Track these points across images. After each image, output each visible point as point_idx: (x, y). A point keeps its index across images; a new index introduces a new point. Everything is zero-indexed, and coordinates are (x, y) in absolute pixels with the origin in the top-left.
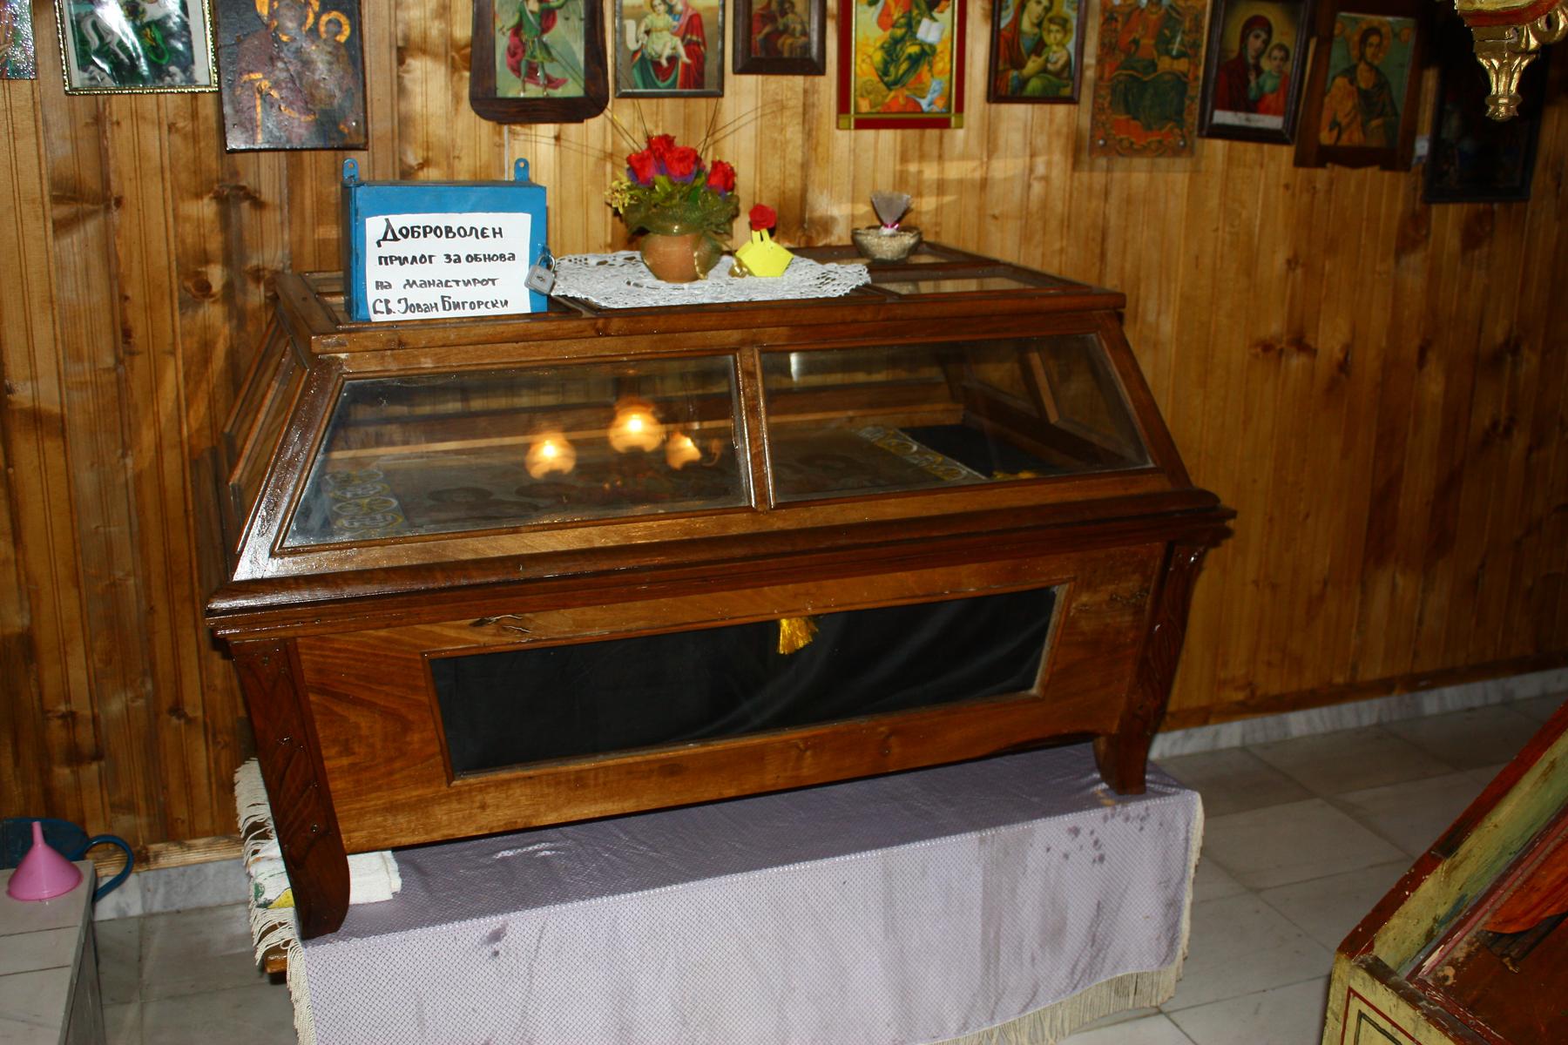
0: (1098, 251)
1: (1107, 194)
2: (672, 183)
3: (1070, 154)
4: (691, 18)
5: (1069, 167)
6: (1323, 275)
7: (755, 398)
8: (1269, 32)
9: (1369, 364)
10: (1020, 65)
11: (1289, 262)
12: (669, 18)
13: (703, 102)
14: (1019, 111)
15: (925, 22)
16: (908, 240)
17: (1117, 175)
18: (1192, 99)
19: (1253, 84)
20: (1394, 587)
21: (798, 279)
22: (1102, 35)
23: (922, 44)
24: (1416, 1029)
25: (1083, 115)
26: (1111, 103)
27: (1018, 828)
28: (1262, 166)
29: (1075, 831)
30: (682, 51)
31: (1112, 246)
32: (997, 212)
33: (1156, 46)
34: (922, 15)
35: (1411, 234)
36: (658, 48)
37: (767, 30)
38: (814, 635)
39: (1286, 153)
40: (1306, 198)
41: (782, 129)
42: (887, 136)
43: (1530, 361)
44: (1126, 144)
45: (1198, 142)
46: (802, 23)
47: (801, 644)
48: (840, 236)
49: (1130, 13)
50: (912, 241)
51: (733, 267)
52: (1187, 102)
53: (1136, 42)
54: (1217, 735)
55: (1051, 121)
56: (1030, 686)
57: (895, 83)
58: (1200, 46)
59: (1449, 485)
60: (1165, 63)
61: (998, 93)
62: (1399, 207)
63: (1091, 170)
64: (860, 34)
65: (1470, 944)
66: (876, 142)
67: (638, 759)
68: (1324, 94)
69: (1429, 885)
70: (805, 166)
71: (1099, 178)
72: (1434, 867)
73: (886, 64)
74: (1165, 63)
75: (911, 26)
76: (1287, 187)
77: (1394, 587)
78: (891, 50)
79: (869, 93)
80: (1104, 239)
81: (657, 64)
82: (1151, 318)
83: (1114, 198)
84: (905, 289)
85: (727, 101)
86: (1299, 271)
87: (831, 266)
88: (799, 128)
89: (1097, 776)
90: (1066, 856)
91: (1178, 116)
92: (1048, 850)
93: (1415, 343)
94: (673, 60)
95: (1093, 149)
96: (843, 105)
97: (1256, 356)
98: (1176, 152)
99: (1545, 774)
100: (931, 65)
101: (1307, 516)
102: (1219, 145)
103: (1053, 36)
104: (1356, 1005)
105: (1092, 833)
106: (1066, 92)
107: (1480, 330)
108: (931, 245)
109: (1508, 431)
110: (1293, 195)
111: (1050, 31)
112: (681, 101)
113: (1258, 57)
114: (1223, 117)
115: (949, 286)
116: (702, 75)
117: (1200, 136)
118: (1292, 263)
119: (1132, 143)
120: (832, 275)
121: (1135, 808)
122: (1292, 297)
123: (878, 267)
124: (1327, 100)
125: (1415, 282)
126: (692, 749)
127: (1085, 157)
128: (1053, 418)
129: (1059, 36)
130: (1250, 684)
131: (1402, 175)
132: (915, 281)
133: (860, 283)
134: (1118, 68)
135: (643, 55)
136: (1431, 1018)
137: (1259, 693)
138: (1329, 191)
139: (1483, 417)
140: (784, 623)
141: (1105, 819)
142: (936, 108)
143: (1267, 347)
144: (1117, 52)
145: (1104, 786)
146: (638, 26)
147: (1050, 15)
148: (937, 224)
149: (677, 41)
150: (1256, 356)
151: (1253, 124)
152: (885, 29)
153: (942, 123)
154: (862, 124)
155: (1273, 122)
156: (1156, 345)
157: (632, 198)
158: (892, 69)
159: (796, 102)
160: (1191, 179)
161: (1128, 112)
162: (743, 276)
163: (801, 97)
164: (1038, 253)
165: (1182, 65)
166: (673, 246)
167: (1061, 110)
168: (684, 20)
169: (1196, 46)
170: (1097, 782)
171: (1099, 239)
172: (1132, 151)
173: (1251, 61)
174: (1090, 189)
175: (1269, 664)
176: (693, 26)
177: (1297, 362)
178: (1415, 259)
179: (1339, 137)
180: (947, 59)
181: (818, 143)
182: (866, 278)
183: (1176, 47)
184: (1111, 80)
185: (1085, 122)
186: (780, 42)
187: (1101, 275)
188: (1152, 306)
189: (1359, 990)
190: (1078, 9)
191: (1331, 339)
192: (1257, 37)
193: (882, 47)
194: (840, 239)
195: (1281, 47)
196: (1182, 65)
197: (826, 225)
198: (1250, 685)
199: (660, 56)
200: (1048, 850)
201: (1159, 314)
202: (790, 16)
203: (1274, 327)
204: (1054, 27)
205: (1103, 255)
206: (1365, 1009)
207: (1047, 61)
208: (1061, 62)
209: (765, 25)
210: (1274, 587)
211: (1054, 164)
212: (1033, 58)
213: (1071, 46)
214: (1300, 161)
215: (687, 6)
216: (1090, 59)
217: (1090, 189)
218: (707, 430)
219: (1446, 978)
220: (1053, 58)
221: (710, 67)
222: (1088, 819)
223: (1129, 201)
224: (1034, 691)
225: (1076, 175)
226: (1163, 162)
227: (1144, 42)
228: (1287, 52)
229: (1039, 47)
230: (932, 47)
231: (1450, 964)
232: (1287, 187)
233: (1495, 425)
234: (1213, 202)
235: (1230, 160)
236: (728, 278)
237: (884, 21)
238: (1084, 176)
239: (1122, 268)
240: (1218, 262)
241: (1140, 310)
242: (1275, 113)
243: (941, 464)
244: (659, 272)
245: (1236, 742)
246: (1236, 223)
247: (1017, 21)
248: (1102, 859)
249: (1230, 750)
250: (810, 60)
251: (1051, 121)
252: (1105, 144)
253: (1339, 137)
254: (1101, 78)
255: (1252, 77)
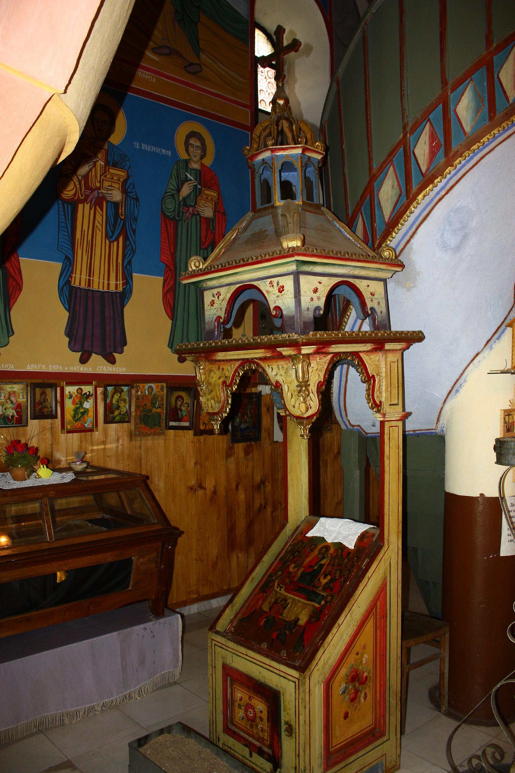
0: (139, 464)
1: (140, 447)
2: (19, 454)
3: (129, 437)
4: (18, 405)
5: (129, 441)
6: (205, 466)
7: (47, 511)
8: (183, 399)
9: (222, 491)
10: (113, 413)
11: (195, 463)
12: (11, 405)
13: (21, 428)
14: (114, 425)
15: (85, 402)
16: (85, 465)
17: (143, 442)
18: (163, 419)
19: (180, 414)
20: (238, 557)
21: (55, 478)
22: (136, 403)
23: (85, 409)
24: (226, 643)
25: (132, 426)
26: (140, 422)
27: (129, 629)
28: (184, 436)
29: (145, 629)
30: (15, 414)
31: (143, 462)
32: (109, 455)
33: (151, 405)
34: (84, 401)
35: (229, 453)
36: (8, 413)
37: (40, 407)
38: (67, 576)
39: (191, 432)
40: (198, 445)
41: (45, 435)
42: (76, 435)
43: (269, 486)
44: (145, 433)
45: (166, 431)
46: (50, 404)
47: (63, 579)
48: (63, 465)
49: (143, 397)
50: (86, 465)
51: (36, 476)
52: (161, 420)
53: (146, 405)
54: (190, 609)
55: (123, 428)
56: (129, 587)
57: (78, 420)
58: (163, 405)
59: (250, 525)
60: (154, 410)
61: (107, 421)
62: (225, 445)
63: (135, 441)
64: (67, 406)
65: (237, 622)
66: (73, 437)
67: (18, 617)
68: (200, 416)
69: (227, 611)
70: (52, 445)
71: (138, 443)
72: (228, 606)
73: (75, 415)
74: (154, 410)
75: (81, 404)
76: (192, 442)
77: (238, 557)
78: (76, 411)
79: (70, 423)
80: (141, 461)
81: (8, 418)
82: (156, 482)
83: (143, 447)
84: (85, 479)
85: (29, 428)
86: (198, 466)
87: (64, 474)
88: (50, 434)
89: (151, 614)
90: (143, 636)
91: (159, 424)
92: (138, 635)
93: (234, 484)
94: (13, 416)
95: (135, 435)
96: (63, 427)
97: (188, 491)
98: (160, 434)
99: (251, 581)
100: (87, 414)
101: (209, 538)
102: (172, 431)
103: (122, 405)
104: (214, 642)
105: (150, 629)
106: (127, 419)
107: (253, 478)
108: (90, 466)
109: (265, 507)
110: (194, 444)
111: (121, 403)
112: (15, 428)
113: (180, 406)
114: (172, 424)
115: (96, 478)
116: (21, 420)
117: (166, 429)
118: (196, 463)
119: (147, 433)
120: (65, 477)
121: (162, 620)
122: (197, 474)
123: (76, 473)
124: (201, 417)
125: (232, 466)
126: (34, 613)
127: (133, 438)
128: (129, 512)
129: (124, 404)
130: (198, 592)
131: (225, 436)
132: (87, 476)
133: (73, 478)
134: (141, 412)
135: (4, 416)
136: (229, 639)
137: (201, 595)
138: (205, 442)
139: (257, 505)
140: (58, 573)
141: (154, 624)
142: (90, 426)
143: (191, 488)
144: (140, 408)
145: (153, 616)
146: (2, 407)
147: (120, 399)
148: (91, 459)
149: (14, 411)
150: (188, 491)
151: (181, 425)
152: (74, 405)
153: (91, 430)
154: (69, 432)
155: (187, 424)
156: (159, 490)
157: (6, 458)
158: (76, 416)
159: (49, 426)
160: (164, 441)
161: (145, 424)
162: (39, 478)
163: (50, 425)
164: (122, 466)
165: (159, 410)
166: (19, 471)
167: (126, 425)
168: (16, 405)
169: (162, 405)
170: (150, 615)
171: (139, 460)
172: (147, 435)
173: (179, 408)
174: (136, 447)
175: (203, 585)
176: (19, 407)
177: (201, 492)
178: (232, 459)
179: (206, 427)
180: (92, 412)
181: (56, 438)
182: (74, 477)
183: (157, 405)
184: (139, 415)
185: (133, 428)
186: (44, 410)
187: (141, 471)
188: (156, 479)
189: (214, 638)
190: (129, 396)
191: (209, 484)
192: (180, 401)
193: (73, 410)
194: (63, 465)
195: (187, 403)
196: (159, 410)
197: (59, 462)
198: (198, 592)
199: (9, 416)
200: (138, 635)
201: (159, 481)
202: (47, 403)
203: (193, 482)
204: (122, 402)
205: (141, 465)
206: (216, 643)
207: (121, 411)
208: (125, 411)
209: (39, 406)
210: (202, 561)
211: (124, 441)
212: (117, 411)
213: (127, 407)
214: (195, 434)
215: (17, 401)
216: (133, 409)
217: (136, 447)
218: (26, 525)
219: (232, 630)
220: (122, 410)
221: (24, 418)
222: (149, 625)
223: (147, 449)
224: (130, 588)
225: (131, 443)
226: (156, 437)
227: (148, 404)
228: (188, 404)
229: (118, 407)
230: (88, 409)
231: (233, 627)
232: (192, 442)
233: (261, 506)
234: (172, 448)
235: (175, 436)
236: (35, 479)
237: (74, 403)
238: (134, 443)
239: (147, 469)
240: (175, 464)
241: (153, 480)
242: (187, 422)
243: (98, 528)
244: (15, 478)
245: (196, 611)
246: (179, 453)
247: (111, 400)
248: (154, 636)
249: (194, 614)
250: (53, 415)
251: (123, 428)
252: (139, 434)
253: (206, 427)
254: (136, 415)
255: (179, 412)
